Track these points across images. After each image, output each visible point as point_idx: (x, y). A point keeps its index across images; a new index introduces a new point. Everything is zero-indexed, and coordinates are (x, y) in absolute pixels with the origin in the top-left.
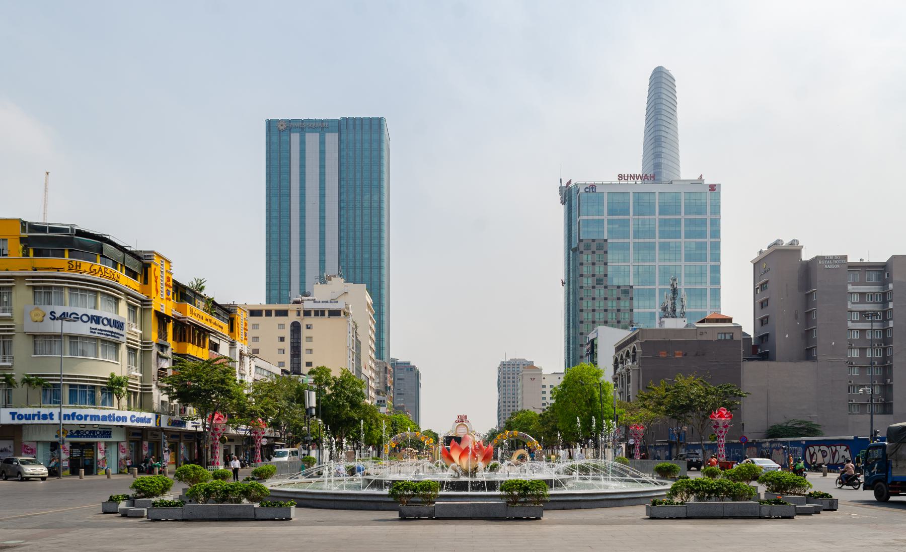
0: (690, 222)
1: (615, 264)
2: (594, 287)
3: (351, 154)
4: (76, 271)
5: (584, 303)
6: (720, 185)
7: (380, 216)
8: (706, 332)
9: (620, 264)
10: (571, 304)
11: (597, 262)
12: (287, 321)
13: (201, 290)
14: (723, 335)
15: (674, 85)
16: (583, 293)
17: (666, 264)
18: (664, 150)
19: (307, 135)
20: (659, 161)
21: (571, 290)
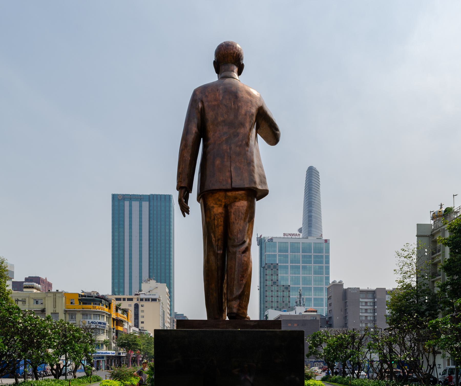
0: (316, 257)
1: (282, 275)
2: (272, 286)
3: (155, 212)
4: (95, 309)
5: (268, 293)
6: (329, 240)
7: (170, 244)
8: (306, 316)
9: (284, 275)
10: (262, 293)
11: (273, 274)
12: (133, 303)
13: (120, 306)
14: (313, 318)
15: (319, 178)
16: (267, 288)
17: (305, 275)
18: (313, 209)
19: (133, 202)
20: (311, 214)
21: (262, 286)
